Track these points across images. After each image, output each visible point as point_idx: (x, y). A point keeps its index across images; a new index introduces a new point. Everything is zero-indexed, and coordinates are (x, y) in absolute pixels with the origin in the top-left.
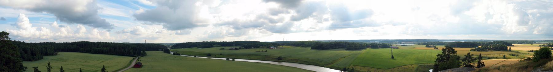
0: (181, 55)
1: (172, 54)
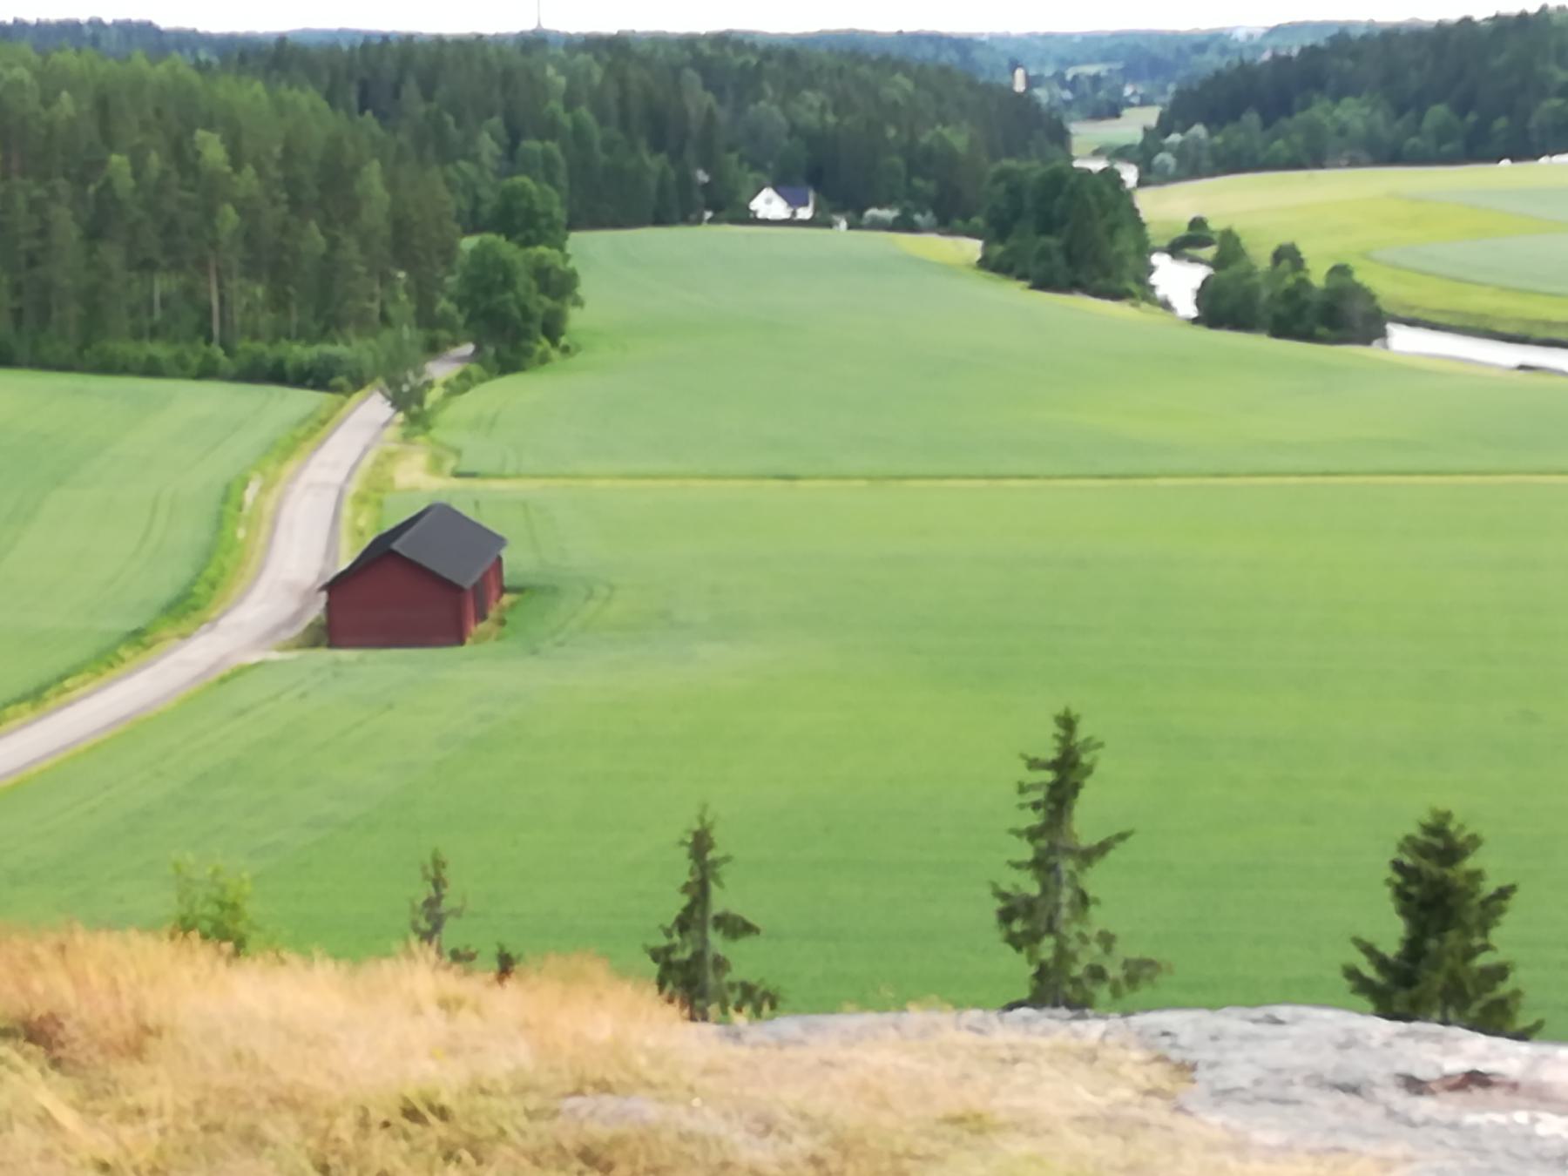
0: (1402, 339)
1: (1187, 307)
